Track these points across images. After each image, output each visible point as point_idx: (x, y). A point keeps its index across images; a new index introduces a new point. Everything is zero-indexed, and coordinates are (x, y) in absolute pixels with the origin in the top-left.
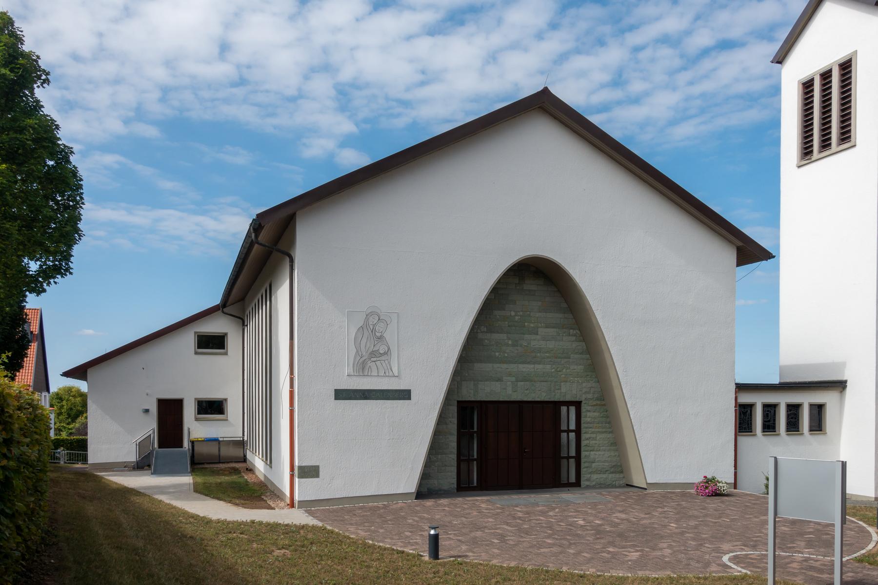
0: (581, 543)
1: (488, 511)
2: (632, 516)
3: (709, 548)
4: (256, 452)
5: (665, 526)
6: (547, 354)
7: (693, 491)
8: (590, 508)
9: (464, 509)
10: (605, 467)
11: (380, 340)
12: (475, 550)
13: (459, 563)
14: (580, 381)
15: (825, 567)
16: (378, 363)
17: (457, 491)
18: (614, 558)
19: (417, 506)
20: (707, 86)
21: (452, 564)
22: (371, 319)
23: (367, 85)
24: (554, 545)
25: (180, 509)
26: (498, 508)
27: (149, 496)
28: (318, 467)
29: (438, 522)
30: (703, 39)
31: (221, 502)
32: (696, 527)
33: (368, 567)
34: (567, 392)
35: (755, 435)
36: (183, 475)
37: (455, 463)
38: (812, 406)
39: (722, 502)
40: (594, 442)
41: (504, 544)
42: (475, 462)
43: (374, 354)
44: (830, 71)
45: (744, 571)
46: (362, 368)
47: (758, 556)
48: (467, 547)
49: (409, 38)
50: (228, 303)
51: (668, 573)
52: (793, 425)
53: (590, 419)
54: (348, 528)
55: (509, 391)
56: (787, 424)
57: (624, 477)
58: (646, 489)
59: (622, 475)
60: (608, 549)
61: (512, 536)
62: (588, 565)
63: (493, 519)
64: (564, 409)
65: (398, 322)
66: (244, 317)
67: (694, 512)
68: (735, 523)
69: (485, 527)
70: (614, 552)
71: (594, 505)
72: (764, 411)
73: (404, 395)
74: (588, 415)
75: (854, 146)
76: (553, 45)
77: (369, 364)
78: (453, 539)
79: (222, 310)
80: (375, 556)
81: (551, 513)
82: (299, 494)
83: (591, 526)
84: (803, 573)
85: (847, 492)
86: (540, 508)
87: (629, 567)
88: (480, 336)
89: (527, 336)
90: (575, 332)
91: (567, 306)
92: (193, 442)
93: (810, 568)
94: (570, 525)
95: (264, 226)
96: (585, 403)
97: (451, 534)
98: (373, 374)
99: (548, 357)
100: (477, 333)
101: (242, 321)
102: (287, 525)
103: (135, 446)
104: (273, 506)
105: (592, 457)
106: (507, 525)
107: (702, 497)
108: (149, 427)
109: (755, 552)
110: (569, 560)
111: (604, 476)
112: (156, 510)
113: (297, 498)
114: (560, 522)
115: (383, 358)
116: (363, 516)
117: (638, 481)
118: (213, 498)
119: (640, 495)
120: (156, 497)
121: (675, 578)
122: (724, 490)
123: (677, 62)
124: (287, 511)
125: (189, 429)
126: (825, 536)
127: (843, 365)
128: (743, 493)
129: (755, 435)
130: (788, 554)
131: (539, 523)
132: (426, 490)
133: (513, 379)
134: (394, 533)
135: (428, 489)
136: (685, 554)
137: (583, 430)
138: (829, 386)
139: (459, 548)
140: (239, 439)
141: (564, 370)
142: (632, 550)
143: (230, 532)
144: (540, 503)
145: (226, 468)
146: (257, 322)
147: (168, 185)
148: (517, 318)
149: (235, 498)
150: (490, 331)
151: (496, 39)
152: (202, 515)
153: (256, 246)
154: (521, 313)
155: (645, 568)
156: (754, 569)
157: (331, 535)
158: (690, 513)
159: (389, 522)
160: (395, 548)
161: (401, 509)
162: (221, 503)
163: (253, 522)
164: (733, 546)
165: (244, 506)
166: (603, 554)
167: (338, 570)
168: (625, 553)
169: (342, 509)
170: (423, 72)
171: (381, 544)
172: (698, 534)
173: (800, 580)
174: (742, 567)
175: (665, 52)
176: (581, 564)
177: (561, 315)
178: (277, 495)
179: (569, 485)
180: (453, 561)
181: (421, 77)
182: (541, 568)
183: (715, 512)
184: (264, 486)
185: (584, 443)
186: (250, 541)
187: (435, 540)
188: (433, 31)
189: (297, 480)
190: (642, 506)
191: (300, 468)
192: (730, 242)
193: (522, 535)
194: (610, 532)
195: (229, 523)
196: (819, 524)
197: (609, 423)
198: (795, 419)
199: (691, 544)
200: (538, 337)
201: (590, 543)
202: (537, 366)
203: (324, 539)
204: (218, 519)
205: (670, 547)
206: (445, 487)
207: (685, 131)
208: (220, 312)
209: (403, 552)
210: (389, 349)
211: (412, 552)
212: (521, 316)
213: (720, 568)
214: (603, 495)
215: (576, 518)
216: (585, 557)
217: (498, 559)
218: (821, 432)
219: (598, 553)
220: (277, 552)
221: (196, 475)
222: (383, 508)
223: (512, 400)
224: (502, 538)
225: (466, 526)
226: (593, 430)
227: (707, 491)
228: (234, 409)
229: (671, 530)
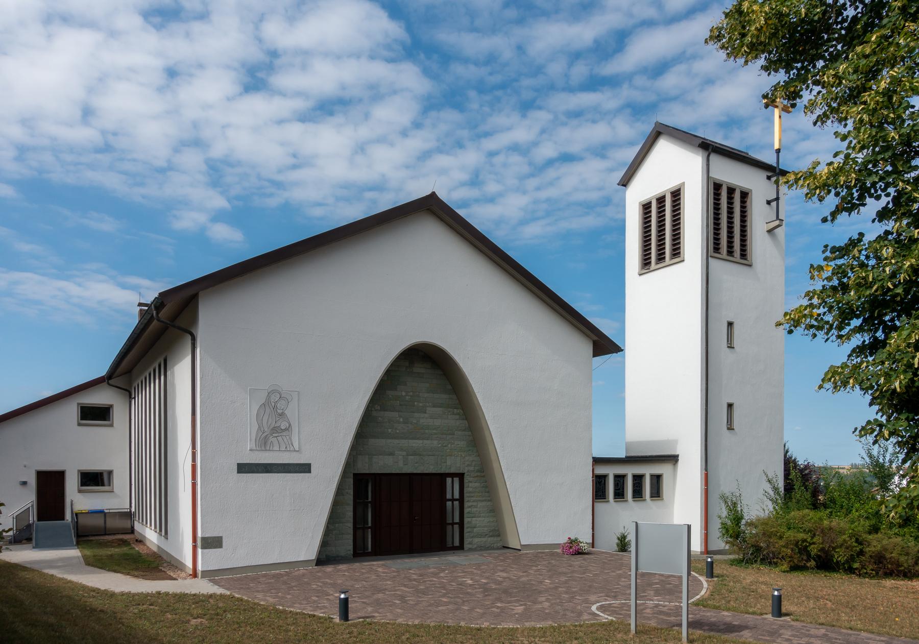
0: (473, 600)
1: (385, 575)
2: (512, 575)
3: (580, 600)
4: (147, 523)
5: (541, 582)
6: (435, 431)
7: (559, 551)
8: (475, 569)
9: (363, 573)
10: (485, 531)
11: (281, 417)
12: (380, 611)
13: (367, 623)
14: (463, 455)
15: (671, 611)
16: (280, 438)
17: (353, 557)
18: (503, 612)
19: (318, 572)
20: (552, 193)
21: (363, 624)
22: (273, 396)
23: (239, 163)
24: (450, 603)
25: (76, 583)
26: (394, 572)
27: (38, 571)
28: (221, 537)
29: (341, 586)
30: (547, 151)
31: (119, 575)
32: (566, 582)
33: (287, 631)
34: (451, 465)
35: (608, 501)
36: (69, 548)
37: (351, 531)
38: (652, 476)
39: (584, 560)
40: (475, 509)
41: (405, 604)
42: (370, 530)
43: (276, 430)
44: (664, 197)
45: (610, 618)
46: (263, 443)
47: (619, 605)
48: (372, 608)
49: (281, 122)
50: (114, 376)
51: (550, 623)
52: (638, 493)
53: (472, 489)
54: (256, 595)
55: (401, 464)
56: (633, 492)
57: (501, 540)
58: (520, 550)
59: (499, 539)
60: (497, 605)
61: (411, 597)
62: (482, 620)
63: (391, 582)
64: (449, 480)
65: (298, 400)
66: (131, 389)
67: (563, 569)
68: (597, 578)
69: (386, 589)
70: (502, 607)
71: (478, 566)
72: (615, 481)
73: (305, 468)
74: (471, 485)
75: (683, 261)
76: (417, 143)
77: (271, 439)
78: (358, 602)
79: (108, 381)
80: (290, 620)
81: (442, 575)
82: (202, 564)
83: (478, 584)
84: (655, 617)
85: (692, 549)
86: (431, 570)
87: (517, 620)
88: (374, 414)
89: (416, 414)
90: (458, 411)
91: (451, 388)
92: (76, 514)
93: (660, 613)
94: (461, 585)
95: (166, 305)
96: (468, 475)
97: (355, 597)
98: (275, 449)
99: (436, 434)
100: (372, 411)
101: (128, 393)
102: (195, 595)
103: (12, 520)
104: (174, 576)
105: (473, 523)
106: (405, 587)
107: (567, 556)
108: (27, 500)
109: (617, 602)
110: (465, 616)
111: (484, 539)
112: (51, 585)
113: (200, 568)
114: (451, 582)
115: (284, 434)
116: (268, 583)
117: (513, 543)
118: (109, 570)
119: (516, 556)
120: (46, 571)
121: (556, 627)
122: (585, 549)
123: (526, 169)
124: (190, 581)
125: (72, 501)
126: (668, 586)
127: (675, 442)
128: (600, 551)
129: (608, 501)
130: (642, 602)
131: (433, 584)
132: (325, 557)
133: (404, 453)
134: (301, 599)
135: (326, 556)
136: (562, 606)
137: (466, 499)
138: (665, 460)
139: (366, 610)
140: (126, 510)
141: (449, 446)
142: (517, 605)
143: (139, 605)
144: (431, 566)
145: (113, 540)
146: (148, 396)
147: (25, 247)
149: (133, 570)
150: (384, 409)
151: (364, 132)
152: (103, 588)
153: (155, 322)
154: (411, 394)
155: (530, 619)
156: (618, 616)
157: (241, 603)
158: (560, 570)
159: (295, 588)
160: (306, 613)
161: (304, 575)
162: (119, 576)
163: (159, 593)
164: (598, 597)
165: (145, 577)
166: (492, 609)
167: (259, 636)
168: (511, 607)
169: (245, 577)
170: (295, 156)
171: (292, 609)
172: (569, 588)
173: (654, 623)
174: (608, 615)
175: (515, 158)
176: (476, 619)
178: (177, 565)
179: (454, 549)
180: (363, 622)
181: (291, 161)
182: (442, 624)
183: (580, 569)
184: (158, 557)
185: (466, 510)
186: (163, 612)
187: (345, 604)
188: (303, 118)
189: (200, 551)
190: (519, 565)
191: (203, 539)
192: (588, 336)
193: (420, 595)
194: (495, 589)
195: (134, 595)
196: (662, 575)
197: (488, 492)
198: (640, 487)
199: (564, 597)
200: (426, 415)
201: (481, 600)
202: (425, 442)
203: (236, 607)
204: (122, 592)
205: (548, 600)
206: (343, 553)
207: (533, 230)
208: (105, 384)
209: (314, 616)
210: (290, 425)
211: (322, 615)
212: (411, 396)
213: (591, 616)
214: (485, 557)
215: (464, 578)
216: (478, 612)
217: (402, 618)
218: (659, 498)
219: (489, 608)
220: (193, 622)
221: (83, 548)
222: (286, 575)
223: (403, 472)
224: (402, 598)
225: (367, 589)
226: (474, 498)
227: (571, 550)
228: (120, 481)
229: (546, 586)
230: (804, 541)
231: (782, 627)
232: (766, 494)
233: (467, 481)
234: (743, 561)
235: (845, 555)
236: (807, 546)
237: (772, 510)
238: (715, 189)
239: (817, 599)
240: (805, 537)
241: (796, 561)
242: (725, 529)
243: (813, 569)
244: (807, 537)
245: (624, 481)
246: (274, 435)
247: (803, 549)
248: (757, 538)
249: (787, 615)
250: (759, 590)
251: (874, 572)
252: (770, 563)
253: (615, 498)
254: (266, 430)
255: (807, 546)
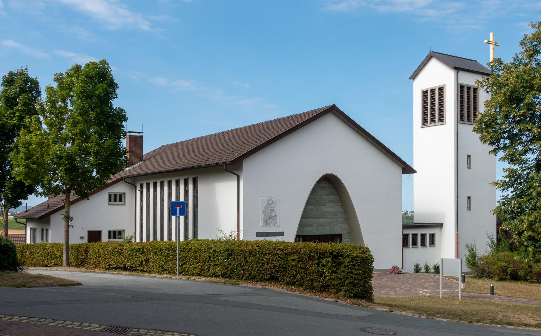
6: (329, 214)
38: (430, 234)
46: (266, 223)
52: (423, 243)
72: (412, 237)
75: (445, 124)
89: (321, 206)
99: (330, 215)
115: (274, 218)
133: (317, 225)
141: (336, 221)
148: (318, 198)
177: (334, 197)
192: (400, 165)
200: (326, 207)
202: (325, 219)
227: (395, 272)
230: (505, 266)
231: (493, 297)
232: (488, 244)
233: (343, 238)
234: (477, 276)
235: (524, 273)
236: (506, 269)
237: (490, 252)
238: (460, 88)
239: (509, 289)
240: (505, 265)
241: (501, 276)
242: (468, 262)
243: (509, 279)
244: (506, 264)
245: (416, 237)
246: (270, 219)
247: (504, 270)
248: (484, 265)
249: (495, 294)
250: (485, 287)
251: (536, 281)
252: (490, 277)
253: (412, 246)
254: (267, 217)
255: (506, 269)
